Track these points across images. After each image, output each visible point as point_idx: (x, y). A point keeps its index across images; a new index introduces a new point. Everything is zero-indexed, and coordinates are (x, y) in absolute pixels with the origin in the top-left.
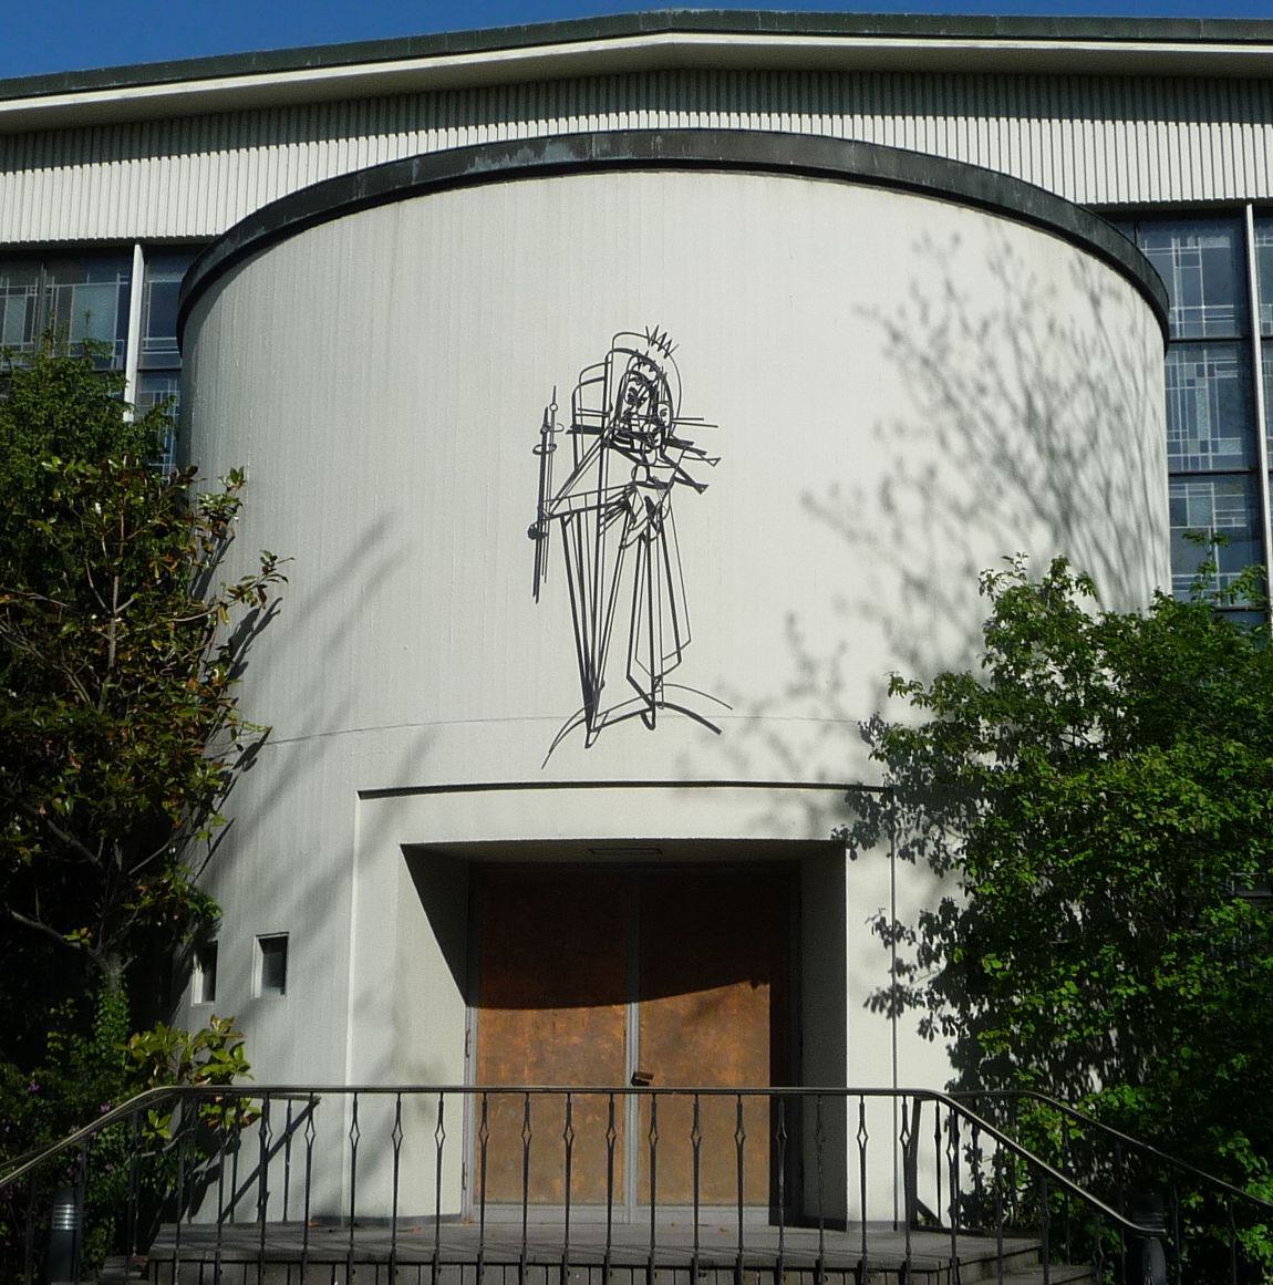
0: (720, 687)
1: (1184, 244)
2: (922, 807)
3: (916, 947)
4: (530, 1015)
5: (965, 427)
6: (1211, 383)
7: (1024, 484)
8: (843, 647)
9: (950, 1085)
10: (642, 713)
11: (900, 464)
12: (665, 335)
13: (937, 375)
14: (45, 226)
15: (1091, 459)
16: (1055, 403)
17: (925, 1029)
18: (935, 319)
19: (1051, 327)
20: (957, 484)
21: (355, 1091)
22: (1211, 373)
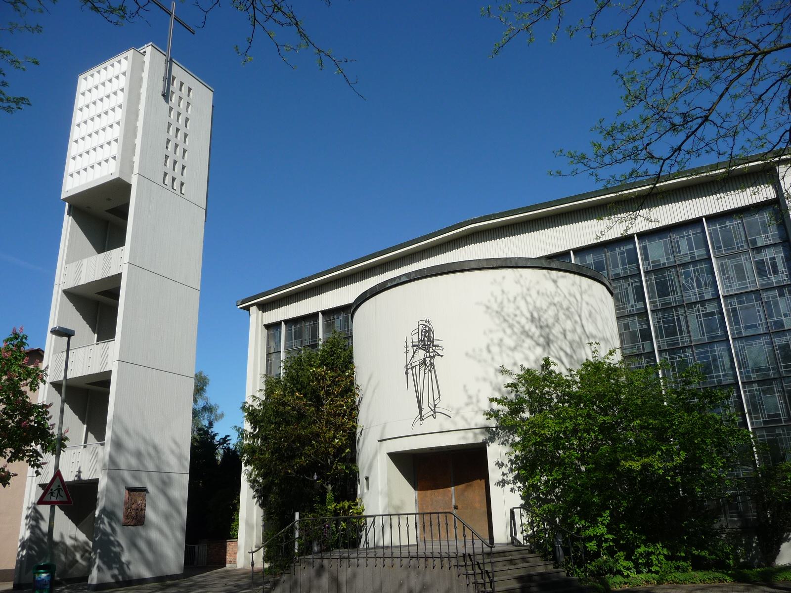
0: (448, 407)
1: (620, 249)
2: (507, 430)
3: (508, 468)
4: (429, 492)
5: (511, 326)
6: (632, 287)
7: (532, 338)
8: (479, 391)
9: (521, 505)
10: (432, 415)
11: (492, 340)
14: (546, 251)
15: (557, 324)
16: (541, 313)
17: (512, 490)
18: (499, 300)
19: (538, 293)
20: (510, 342)
21: (382, 515)
22: (632, 285)
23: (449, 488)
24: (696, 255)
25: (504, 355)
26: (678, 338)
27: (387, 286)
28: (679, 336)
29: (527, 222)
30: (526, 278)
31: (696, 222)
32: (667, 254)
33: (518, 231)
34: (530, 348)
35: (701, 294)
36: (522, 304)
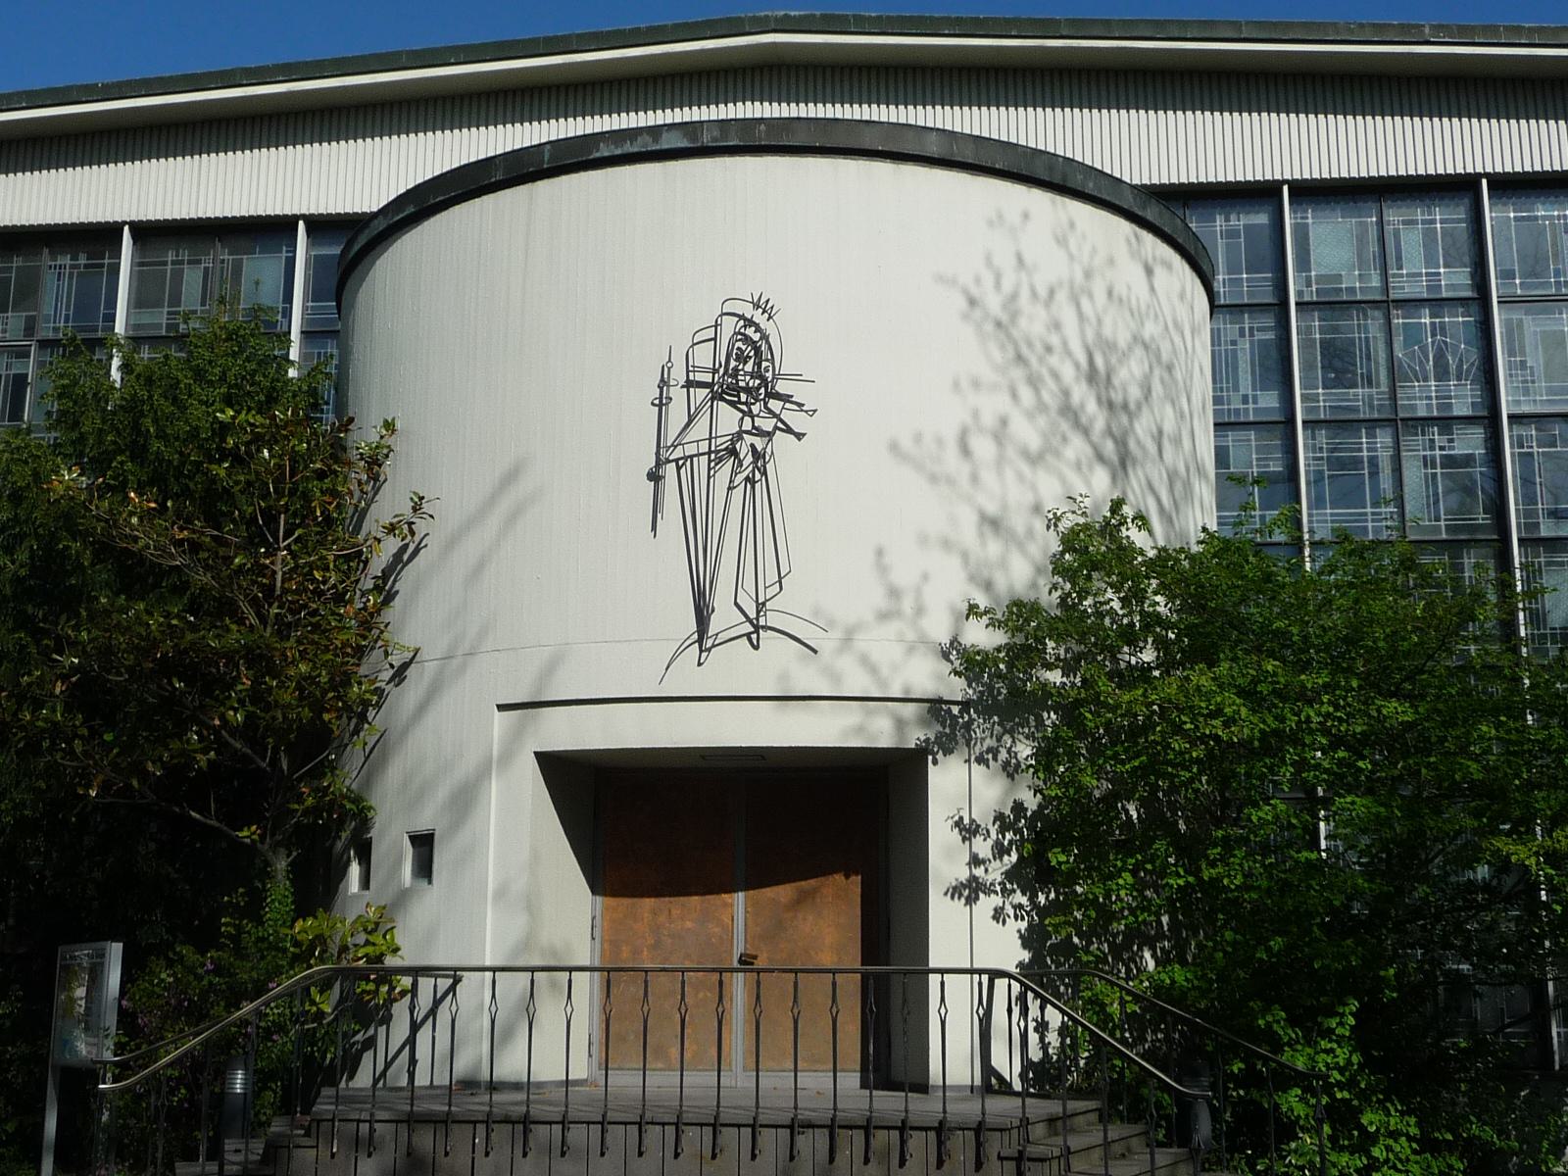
1: (1227, 220)
2: (996, 718)
3: (990, 842)
4: (649, 903)
5: (1034, 382)
6: (1252, 343)
7: (1086, 432)
8: (925, 577)
9: (1020, 965)
10: (748, 635)
11: (976, 414)
12: (768, 301)
13: (1009, 336)
15: (1145, 410)
16: (1114, 360)
17: (998, 915)
18: (1007, 286)
19: (1110, 293)
20: (1027, 433)
21: (494, 970)
22: (1252, 335)
23: (725, 896)
24: (1443, 283)
25: (1009, 474)
26: (1366, 514)
27: (598, 155)
28: (1369, 510)
29: (951, 70)
30: (1084, 237)
31: (1459, 187)
32: (1362, 263)
33: (883, 90)
34: (1078, 466)
35: (1444, 398)
36: (1068, 317)
